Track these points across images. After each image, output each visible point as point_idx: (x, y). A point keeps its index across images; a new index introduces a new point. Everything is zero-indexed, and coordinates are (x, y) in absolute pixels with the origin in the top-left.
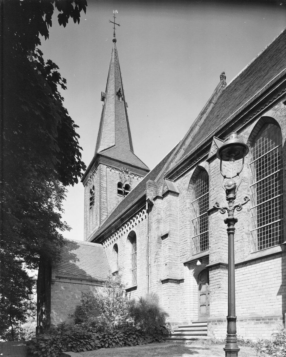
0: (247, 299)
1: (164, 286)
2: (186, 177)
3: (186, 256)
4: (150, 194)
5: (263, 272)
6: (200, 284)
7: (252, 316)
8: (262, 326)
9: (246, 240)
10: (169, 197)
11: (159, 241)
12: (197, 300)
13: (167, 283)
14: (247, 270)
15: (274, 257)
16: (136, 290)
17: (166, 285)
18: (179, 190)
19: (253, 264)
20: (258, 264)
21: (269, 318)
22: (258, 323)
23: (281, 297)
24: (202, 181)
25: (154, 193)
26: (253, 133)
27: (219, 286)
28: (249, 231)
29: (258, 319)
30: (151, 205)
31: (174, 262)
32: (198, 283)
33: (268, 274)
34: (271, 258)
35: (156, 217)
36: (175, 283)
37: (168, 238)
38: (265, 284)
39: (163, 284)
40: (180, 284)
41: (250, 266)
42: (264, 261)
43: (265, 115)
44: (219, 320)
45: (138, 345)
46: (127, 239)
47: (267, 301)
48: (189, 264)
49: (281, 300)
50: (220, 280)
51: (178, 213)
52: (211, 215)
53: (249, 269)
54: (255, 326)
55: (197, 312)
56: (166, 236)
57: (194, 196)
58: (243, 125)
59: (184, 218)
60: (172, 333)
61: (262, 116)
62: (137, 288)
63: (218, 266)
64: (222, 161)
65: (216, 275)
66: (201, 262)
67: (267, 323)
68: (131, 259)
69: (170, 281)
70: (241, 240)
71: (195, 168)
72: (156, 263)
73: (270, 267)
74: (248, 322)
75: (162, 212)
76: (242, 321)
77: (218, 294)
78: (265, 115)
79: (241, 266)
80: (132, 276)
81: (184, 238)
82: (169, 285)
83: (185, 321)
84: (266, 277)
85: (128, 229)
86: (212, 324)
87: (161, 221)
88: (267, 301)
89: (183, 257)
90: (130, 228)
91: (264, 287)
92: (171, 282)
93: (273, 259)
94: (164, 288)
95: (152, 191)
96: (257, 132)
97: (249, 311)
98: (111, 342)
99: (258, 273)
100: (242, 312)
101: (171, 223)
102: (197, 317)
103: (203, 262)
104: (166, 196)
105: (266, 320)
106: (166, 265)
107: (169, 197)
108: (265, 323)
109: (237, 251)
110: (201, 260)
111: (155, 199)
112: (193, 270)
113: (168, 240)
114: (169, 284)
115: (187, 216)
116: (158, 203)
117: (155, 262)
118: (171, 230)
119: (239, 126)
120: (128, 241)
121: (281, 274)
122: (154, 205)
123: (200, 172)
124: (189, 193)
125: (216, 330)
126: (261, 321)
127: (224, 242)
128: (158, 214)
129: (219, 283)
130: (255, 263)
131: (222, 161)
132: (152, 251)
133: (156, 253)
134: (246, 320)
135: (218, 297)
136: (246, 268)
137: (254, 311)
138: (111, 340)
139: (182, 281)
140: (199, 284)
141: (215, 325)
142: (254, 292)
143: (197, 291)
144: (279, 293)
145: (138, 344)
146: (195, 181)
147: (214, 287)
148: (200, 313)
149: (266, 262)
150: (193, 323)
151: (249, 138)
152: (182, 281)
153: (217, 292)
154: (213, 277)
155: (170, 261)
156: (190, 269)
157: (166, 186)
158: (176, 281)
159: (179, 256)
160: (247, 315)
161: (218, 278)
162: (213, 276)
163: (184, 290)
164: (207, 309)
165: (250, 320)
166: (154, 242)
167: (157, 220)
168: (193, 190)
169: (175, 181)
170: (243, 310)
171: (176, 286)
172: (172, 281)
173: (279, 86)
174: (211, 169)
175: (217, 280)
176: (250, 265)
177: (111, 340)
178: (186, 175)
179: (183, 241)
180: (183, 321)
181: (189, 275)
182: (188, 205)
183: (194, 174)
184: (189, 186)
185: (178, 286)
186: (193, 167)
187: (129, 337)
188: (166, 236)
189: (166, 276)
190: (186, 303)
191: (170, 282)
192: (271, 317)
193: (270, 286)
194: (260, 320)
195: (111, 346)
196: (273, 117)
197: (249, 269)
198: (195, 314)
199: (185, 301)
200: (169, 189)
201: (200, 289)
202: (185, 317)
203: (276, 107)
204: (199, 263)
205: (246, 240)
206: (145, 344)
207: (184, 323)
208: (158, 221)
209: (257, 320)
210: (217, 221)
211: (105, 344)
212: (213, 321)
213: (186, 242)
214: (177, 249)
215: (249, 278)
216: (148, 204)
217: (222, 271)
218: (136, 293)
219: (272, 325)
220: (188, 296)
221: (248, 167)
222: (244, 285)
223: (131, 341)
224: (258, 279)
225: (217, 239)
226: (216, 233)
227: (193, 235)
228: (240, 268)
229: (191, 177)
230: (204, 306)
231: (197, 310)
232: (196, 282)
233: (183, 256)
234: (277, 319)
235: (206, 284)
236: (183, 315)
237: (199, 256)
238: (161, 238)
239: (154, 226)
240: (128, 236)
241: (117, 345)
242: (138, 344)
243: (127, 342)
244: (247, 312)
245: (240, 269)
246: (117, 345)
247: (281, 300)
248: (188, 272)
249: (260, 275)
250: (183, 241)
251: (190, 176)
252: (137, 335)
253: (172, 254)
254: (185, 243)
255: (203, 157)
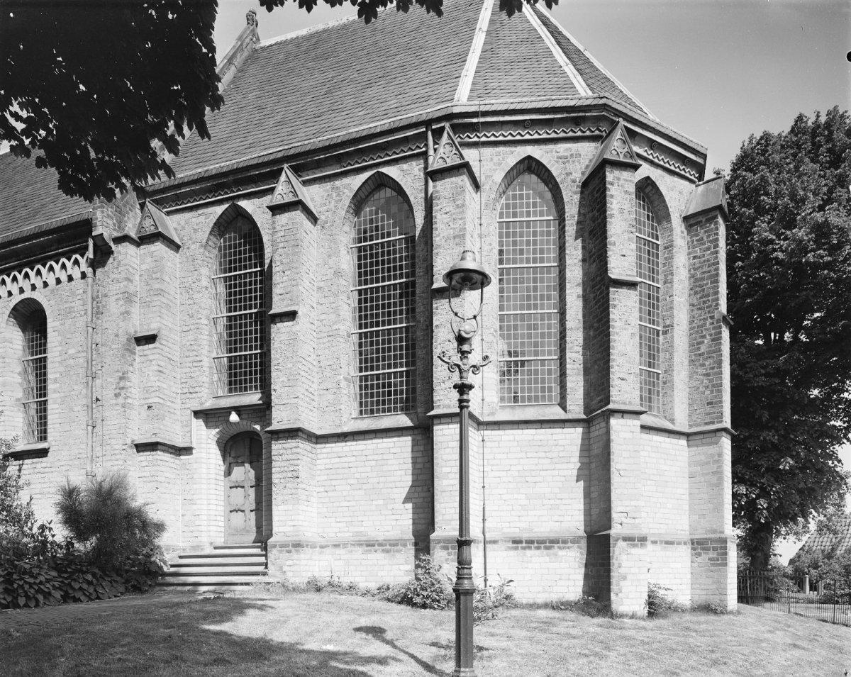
0: (348, 504)
1: (142, 458)
2: (200, 215)
3: (199, 395)
4: (105, 224)
5: (380, 457)
6: (230, 464)
7: (357, 539)
8: (377, 557)
9: (344, 391)
10: (158, 248)
11: (130, 346)
12: (222, 498)
13: (153, 453)
14: (346, 449)
15: (400, 433)
16: (44, 459)
17: (147, 456)
18: (181, 240)
19: (359, 440)
20: (370, 442)
21: (391, 542)
22: (370, 551)
23: (410, 506)
24: (245, 246)
25: (114, 224)
26: (360, 193)
27: (295, 474)
28: (349, 374)
29: (370, 544)
30: (103, 254)
31: (169, 403)
32: (224, 461)
33: (390, 462)
34: (394, 434)
35: (122, 285)
36: (171, 453)
37: (156, 344)
38: (382, 479)
39: (138, 451)
40: (182, 457)
41: (355, 443)
42: (382, 438)
43: (385, 170)
44: (297, 544)
45: (99, 598)
46: (9, 316)
47: (386, 512)
48: (208, 416)
49: (411, 512)
50: (296, 462)
51: (178, 292)
52: (279, 325)
53: (352, 448)
54: (364, 556)
55: (222, 524)
56: (151, 339)
57: (216, 266)
58: (341, 168)
59: (196, 307)
60: (165, 569)
61: (380, 170)
62: (49, 454)
63: (294, 433)
64: (580, 430)
65: (289, 451)
66: (239, 415)
67: (388, 551)
68: (19, 374)
69: (160, 447)
70: (335, 390)
71: (226, 206)
72: (121, 400)
73: (392, 451)
74: (350, 548)
75: (137, 277)
76: (654, 542)
77: (294, 491)
78: (385, 170)
79: (335, 439)
80: (22, 420)
81: (195, 353)
82: (158, 457)
83: (195, 544)
84: (385, 468)
85: (15, 291)
86: (281, 552)
87: (135, 299)
88: (386, 512)
89: (191, 396)
90: (22, 291)
91: (381, 485)
92: (163, 451)
93: (399, 436)
94: (144, 464)
95: (108, 216)
96: (366, 193)
97: (351, 529)
98: (32, 591)
99: (369, 458)
100: (337, 530)
101: (164, 311)
102: (222, 534)
103: (244, 416)
104: (148, 243)
105: (386, 545)
106: (149, 407)
107: (158, 247)
108: (383, 550)
109: (327, 409)
110: (239, 411)
111: (118, 240)
112: (217, 430)
113: (155, 351)
114: (160, 455)
115: (203, 305)
116: (125, 253)
117: (117, 395)
118: (164, 327)
119: (334, 167)
120: (12, 324)
121: (410, 466)
122: (115, 254)
123: (237, 217)
124: (207, 253)
125: (288, 563)
126: (377, 547)
127: (305, 386)
128: (128, 279)
129: (296, 468)
130: (364, 439)
131: (580, 430)
132: (106, 367)
133: (120, 374)
134: (345, 545)
135: (294, 496)
136: (346, 445)
137: (362, 529)
138: (31, 587)
139: (187, 450)
140: (227, 463)
141: (287, 554)
142: (362, 492)
143: (223, 478)
144: (406, 500)
145: (98, 598)
146: (223, 232)
147: (285, 475)
148: (230, 526)
149: (385, 440)
150: (215, 548)
151: (353, 198)
152: (187, 450)
153: (289, 485)
154: (281, 455)
155: (161, 401)
156: (207, 426)
157: (152, 220)
158: (172, 449)
159: (179, 391)
160: (347, 534)
161: (293, 457)
162: (281, 452)
163: (194, 474)
164: (247, 519)
165: (354, 545)
166: (116, 346)
167: (127, 295)
168: (216, 252)
169: (168, 213)
170: (338, 525)
171: (172, 460)
172: (164, 448)
173: (412, 133)
174: (278, 228)
175: (292, 462)
176: (354, 440)
177: (31, 587)
178: (200, 211)
179: (191, 359)
180: (190, 544)
181: (206, 440)
182: (205, 282)
183: (224, 217)
184: (208, 239)
185: (177, 462)
186: (220, 202)
187: (75, 580)
188: (151, 339)
189: (148, 435)
190: (198, 502)
191: (161, 450)
192: (396, 540)
193: (393, 485)
194: (374, 546)
195: (32, 604)
196: (400, 183)
197: (352, 448)
198: (219, 529)
199: (195, 497)
200: (160, 230)
201: (228, 473)
202: (195, 534)
203: (405, 166)
204: (234, 417)
205: (344, 391)
206: (115, 596)
207: (193, 548)
208: (129, 298)
209: (368, 545)
210: (291, 341)
211: (17, 598)
212: (282, 546)
213: (199, 364)
214: (174, 374)
215: (351, 465)
216: (95, 245)
217: (301, 445)
218: (43, 465)
219: (398, 555)
220: (203, 486)
221: (348, 252)
222: (341, 477)
223: (81, 589)
224: (369, 469)
225: (291, 378)
226: (290, 365)
227: (215, 353)
228: (332, 442)
229: (215, 220)
230: (240, 513)
231: (222, 519)
232: (220, 457)
233: (191, 393)
234: (405, 545)
235: (246, 464)
236: (191, 529)
237: (236, 402)
238: (133, 341)
239: (114, 306)
240: (15, 309)
241: (48, 599)
242: (98, 595)
243: (70, 591)
244: (346, 529)
245: (333, 445)
246: (48, 599)
247: (411, 511)
248: (203, 432)
249: (373, 463)
250: (191, 359)
251: (214, 219)
252: (94, 575)
253: (164, 386)
254: (195, 364)
255: (249, 191)
